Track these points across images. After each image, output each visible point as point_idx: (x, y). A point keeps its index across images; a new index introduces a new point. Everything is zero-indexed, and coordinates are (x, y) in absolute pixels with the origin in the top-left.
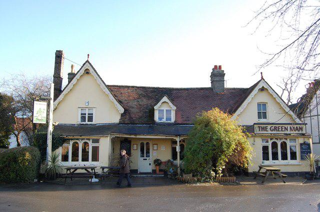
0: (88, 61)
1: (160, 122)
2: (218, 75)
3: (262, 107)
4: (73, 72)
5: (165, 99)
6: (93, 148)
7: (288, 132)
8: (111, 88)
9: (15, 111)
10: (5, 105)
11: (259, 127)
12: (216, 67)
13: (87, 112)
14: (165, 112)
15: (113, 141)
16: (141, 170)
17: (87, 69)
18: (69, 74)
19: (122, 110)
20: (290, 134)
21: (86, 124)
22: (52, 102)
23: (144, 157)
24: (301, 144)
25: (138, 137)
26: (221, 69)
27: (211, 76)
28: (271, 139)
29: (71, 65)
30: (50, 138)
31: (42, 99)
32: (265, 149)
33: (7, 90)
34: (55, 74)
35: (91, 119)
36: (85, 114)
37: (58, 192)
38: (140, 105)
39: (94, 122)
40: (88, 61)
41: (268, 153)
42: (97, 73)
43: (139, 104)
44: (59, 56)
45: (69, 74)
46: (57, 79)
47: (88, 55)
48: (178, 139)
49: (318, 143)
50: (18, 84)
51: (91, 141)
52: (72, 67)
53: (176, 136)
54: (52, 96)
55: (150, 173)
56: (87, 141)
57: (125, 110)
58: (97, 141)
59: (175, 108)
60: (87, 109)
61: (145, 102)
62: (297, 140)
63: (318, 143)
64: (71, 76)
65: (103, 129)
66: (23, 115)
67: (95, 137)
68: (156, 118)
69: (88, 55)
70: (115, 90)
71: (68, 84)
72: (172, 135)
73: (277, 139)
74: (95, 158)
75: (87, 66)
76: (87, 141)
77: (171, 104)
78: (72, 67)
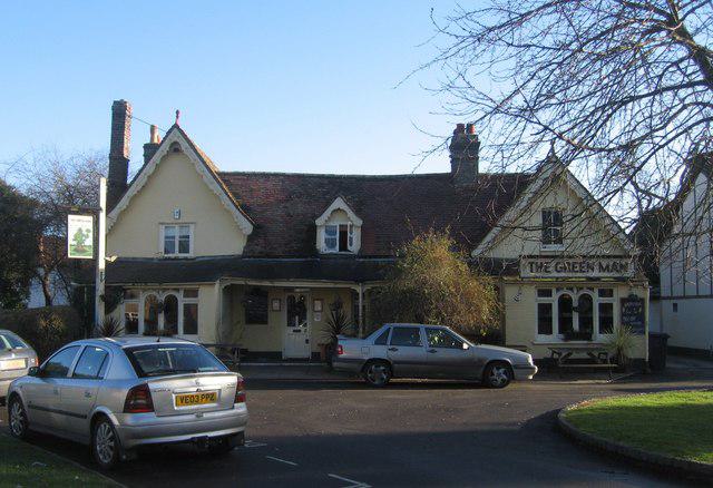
0: (176, 126)
1: (328, 252)
2: (464, 144)
3: (552, 221)
4: (156, 141)
5: (339, 203)
6: (187, 307)
7: (595, 274)
8: (229, 179)
9: (41, 225)
10: (20, 213)
11: (531, 264)
12: (460, 127)
13: (176, 232)
14: (336, 224)
15: (229, 292)
16: (290, 353)
17: (176, 143)
18: (146, 147)
19: (248, 228)
20: (598, 279)
21: (175, 259)
22: (103, 216)
23: (294, 325)
24: (623, 301)
25: (277, 284)
26: (471, 132)
27: (452, 148)
28: (558, 290)
29: (149, 128)
30: (100, 288)
31: (82, 211)
32: (544, 310)
33: (20, 183)
34: (112, 150)
35: (184, 247)
36: (174, 237)
37: (551, 410)
38: (289, 215)
39: (191, 254)
40: (176, 126)
41: (551, 318)
42: (195, 151)
43: (283, 209)
44: (120, 112)
45: (146, 147)
46: (118, 161)
47: (177, 112)
48: (359, 289)
49: (706, 297)
50: (45, 170)
51: (182, 292)
52: (153, 129)
53: (357, 282)
54: (103, 204)
55: (306, 360)
56: (173, 293)
57: (257, 228)
58: (194, 293)
59: (359, 222)
60: (177, 227)
61: (300, 208)
62: (615, 293)
63: (706, 297)
64: (150, 149)
65: (205, 270)
66: (45, 252)
67: (189, 286)
68: (321, 245)
69: (177, 112)
70: (239, 184)
71: (145, 166)
72: (344, 279)
73: (571, 289)
74: (191, 328)
75: (175, 137)
76: (173, 293)
77: (351, 214)
78: (153, 129)
